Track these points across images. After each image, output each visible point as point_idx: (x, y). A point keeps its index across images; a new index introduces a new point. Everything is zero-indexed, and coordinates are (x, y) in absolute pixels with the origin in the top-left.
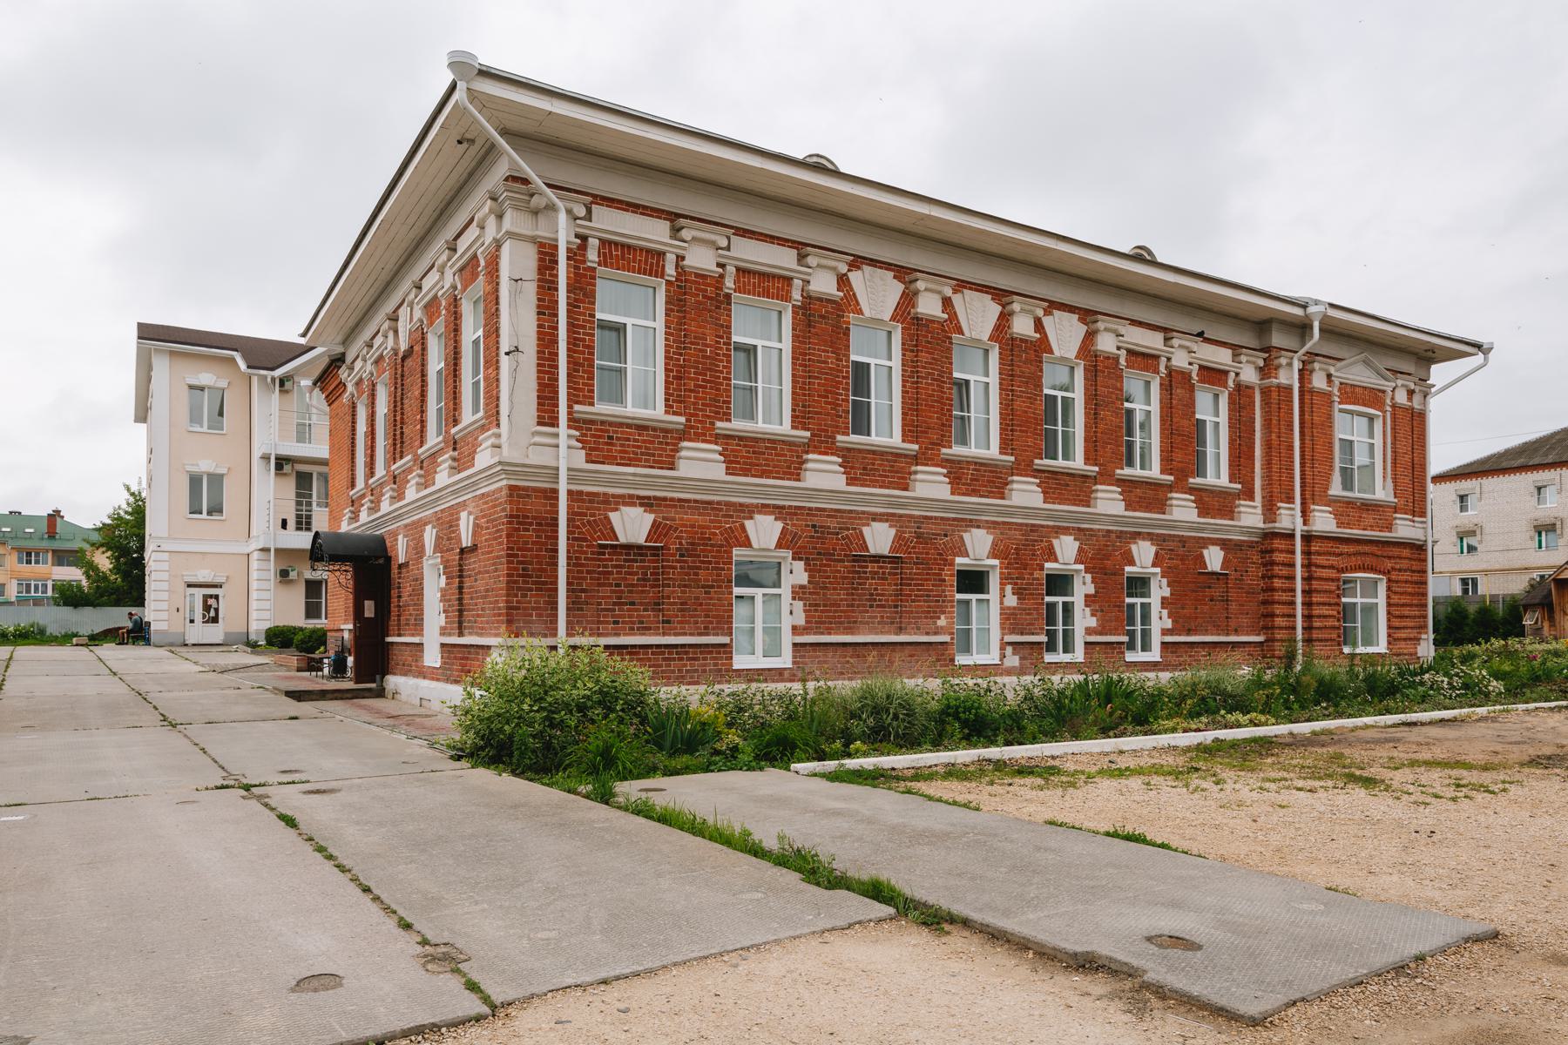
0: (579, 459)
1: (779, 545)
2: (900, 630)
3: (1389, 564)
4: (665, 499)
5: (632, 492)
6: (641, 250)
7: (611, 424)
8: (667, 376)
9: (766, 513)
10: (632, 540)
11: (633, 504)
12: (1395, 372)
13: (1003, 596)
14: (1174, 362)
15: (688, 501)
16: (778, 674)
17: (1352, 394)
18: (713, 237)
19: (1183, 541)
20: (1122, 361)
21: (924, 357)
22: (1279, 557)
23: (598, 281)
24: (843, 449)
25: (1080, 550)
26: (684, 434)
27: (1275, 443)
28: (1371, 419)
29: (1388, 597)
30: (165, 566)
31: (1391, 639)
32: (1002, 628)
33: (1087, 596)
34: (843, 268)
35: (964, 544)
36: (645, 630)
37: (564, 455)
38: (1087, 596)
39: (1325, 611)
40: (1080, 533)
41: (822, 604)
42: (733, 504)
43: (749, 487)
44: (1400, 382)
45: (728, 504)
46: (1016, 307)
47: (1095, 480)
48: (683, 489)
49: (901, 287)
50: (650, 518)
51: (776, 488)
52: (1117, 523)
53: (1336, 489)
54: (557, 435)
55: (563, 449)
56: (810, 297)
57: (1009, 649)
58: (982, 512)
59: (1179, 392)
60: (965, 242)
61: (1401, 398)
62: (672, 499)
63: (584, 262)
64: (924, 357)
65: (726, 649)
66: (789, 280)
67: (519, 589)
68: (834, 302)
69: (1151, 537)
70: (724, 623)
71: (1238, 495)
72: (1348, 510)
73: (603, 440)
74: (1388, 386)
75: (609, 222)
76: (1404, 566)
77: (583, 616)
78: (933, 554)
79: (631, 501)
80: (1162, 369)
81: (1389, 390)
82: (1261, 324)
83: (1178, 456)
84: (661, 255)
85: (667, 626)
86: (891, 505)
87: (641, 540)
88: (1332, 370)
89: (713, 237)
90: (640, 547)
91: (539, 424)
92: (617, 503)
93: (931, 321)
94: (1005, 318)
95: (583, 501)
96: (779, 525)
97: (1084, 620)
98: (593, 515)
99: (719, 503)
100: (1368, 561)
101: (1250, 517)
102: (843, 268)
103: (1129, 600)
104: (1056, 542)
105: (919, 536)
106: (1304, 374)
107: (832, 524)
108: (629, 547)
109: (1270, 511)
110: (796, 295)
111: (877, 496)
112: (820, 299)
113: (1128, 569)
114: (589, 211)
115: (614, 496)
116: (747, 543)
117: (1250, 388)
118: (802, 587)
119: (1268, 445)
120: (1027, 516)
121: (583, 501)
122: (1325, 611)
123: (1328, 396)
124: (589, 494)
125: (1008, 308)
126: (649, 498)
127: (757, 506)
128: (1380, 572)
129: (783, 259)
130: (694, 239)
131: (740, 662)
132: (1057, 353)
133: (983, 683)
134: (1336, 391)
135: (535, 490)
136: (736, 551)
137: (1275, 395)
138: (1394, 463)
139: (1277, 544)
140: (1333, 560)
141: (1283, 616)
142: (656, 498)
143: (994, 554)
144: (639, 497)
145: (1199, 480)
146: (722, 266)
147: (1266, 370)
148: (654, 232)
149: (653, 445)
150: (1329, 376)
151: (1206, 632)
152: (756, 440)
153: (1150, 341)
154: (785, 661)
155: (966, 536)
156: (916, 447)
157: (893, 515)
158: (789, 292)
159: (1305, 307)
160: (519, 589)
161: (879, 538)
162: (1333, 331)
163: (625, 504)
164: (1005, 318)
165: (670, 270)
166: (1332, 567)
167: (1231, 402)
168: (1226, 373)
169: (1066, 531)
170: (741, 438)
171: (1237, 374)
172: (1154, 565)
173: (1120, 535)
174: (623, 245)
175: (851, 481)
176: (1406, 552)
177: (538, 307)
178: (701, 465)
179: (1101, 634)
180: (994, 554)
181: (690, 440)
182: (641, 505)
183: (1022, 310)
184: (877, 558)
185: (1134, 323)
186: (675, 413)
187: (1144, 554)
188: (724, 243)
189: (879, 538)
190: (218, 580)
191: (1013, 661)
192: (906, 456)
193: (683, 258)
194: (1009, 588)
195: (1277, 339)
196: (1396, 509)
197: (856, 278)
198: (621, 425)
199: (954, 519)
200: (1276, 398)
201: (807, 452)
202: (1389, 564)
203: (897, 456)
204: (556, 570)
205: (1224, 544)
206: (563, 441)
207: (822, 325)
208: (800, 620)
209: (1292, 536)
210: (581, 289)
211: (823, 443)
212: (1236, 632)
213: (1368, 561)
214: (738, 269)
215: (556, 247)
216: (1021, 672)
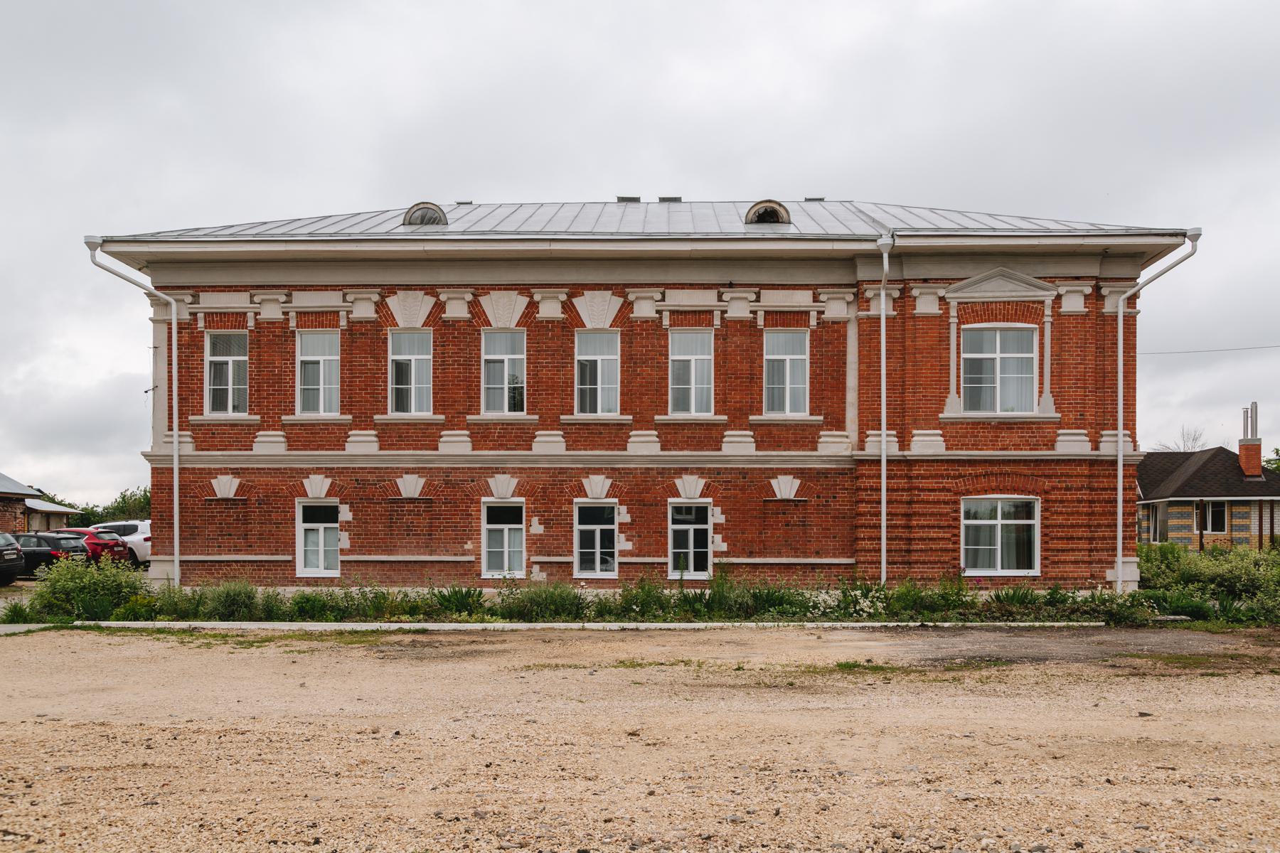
0: (189, 449)
3: (1048, 484)
12: (1051, 279)
16: (330, 581)
18: (744, 295)
19: (744, 473)
21: (451, 349)
31: (1043, 566)
35: (489, 487)
36: (238, 551)
40: (611, 472)
43: (304, 457)
45: (291, 469)
47: (631, 427)
48: (258, 462)
50: (236, 482)
53: (955, 408)
55: (1121, 444)
57: (536, 568)
58: (505, 462)
64: (451, 349)
65: (292, 564)
69: (701, 472)
70: (290, 547)
75: (212, 301)
79: (224, 472)
81: (1049, 302)
82: (850, 261)
85: (249, 549)
87: (231, 496)
89: (744, 295)
93: (456, 322)
96: (797, 482)
104: (585, 481)
106: (903, 301)
108: (227, 500)
110: (343, 323)
111: (407, 456)
114: (663, 294)
123: (941, 321)
131: (301, 572)
132: (589, 325)
133: (698, 591)
134: (953, 313)
139: (864, 470)
140: (946, 483)
150: (942, 299)
151: (779, 555)
152: (313, 425)
154: (336, 573)
158: (338, 321)
161: (411, 486)
165: (717, 322)
169: (597, 471)
170: (302, 425)
173: (662, 472)
175: (291, 447)
178: (455, 445)
179: (638, 556)
184: (411, 500)
195: (863, 273)
196: (1060, 424)
202: (1048, 484)
203: (620, 426)
207: (364, 343)
209: (1114, 463)
211: (643, 422)
213: (1008, 482)
214: (672, 312)
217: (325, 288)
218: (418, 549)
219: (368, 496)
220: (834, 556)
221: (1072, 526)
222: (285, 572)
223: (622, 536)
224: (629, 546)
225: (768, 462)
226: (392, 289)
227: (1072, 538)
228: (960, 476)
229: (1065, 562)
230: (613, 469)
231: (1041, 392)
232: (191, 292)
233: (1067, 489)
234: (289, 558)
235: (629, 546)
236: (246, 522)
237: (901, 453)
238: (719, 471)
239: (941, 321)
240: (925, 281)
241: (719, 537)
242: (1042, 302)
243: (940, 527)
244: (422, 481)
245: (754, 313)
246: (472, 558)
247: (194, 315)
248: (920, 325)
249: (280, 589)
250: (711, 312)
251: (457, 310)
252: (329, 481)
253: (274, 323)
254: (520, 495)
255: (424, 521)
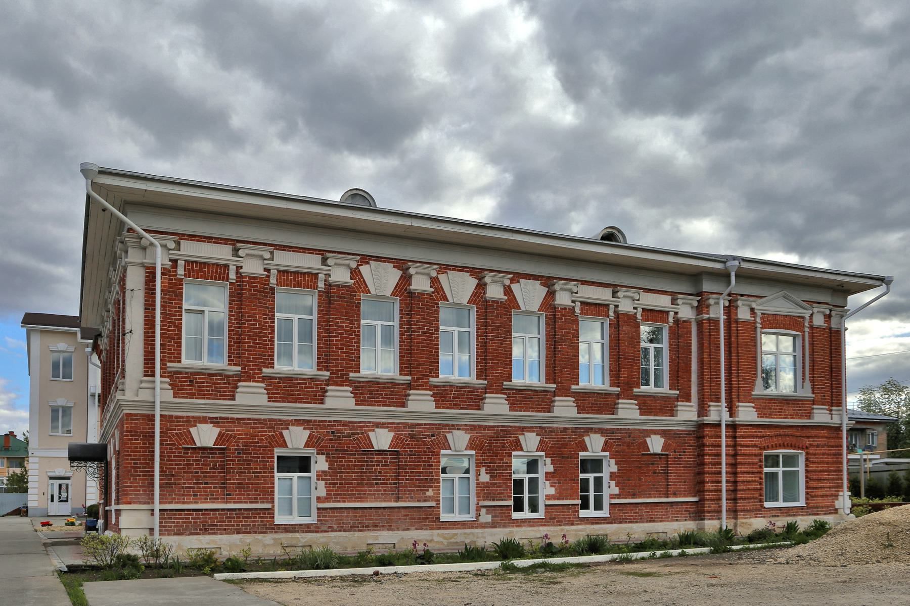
0: (169, 396)
1: (307, 445)
2: (397, 499)
4: (227, 418)
5: (205, 415)
6: (213, 264)
7: (192, 374)
8: (230, 342)
9: (297, 425)
10: (205, 445)
11: (206, 422)
13: (478, 475)
14: (621, 309)
15: (243, 419)
16: (307, 528)
17: (775, 322)
18: (260, 253)
19: (629, 432)
20: (578, 310)
22: (707, 441)
23: (440, 309)
24: (354, 382)
25: (541, 442)
26: (241, 378)
27: (706, 360)
28: (795, 337)
29: (807, 466)
30: (37, 466)
32: (478, 497)
33: (546, 473)
34: (507, 282)
36: (214, 500)
37: (161, 394)
38: (546, 473)
39: (749, 477)
40: (540, 431)
41: (337, 483)
42: (275, 420)
44: (815, 310)
45: (270, 420)
46: (557, 287)
48: (239, 412)
49: (477, 281)
50: (217, 431)
51: (467, 415)
52: (570, 422)
53: (759, 390)
54: (154, 382)
56: (330, 285)
57: (483, 511)
59: (624, 328)
60: (360, 228)
61: (819, 321)
62: (232, 419)
63: (176, 275)
65: (270, 512)
66: (316, 275)
67: (132, 475)
68: (348, 287)
69: (601, 431)
70: (269, 495)
71: (618, 396)
72: (768, 405)
73: (187, 384)
74: (806, 314)
76: (822, 443)
77: (174, 491)
78: (422, 448)
79: (204, 420)
80: (611, 313)
81: (807, 317)
82: (695, 276)
83: (624, 374)
84: (226, 267)
86: (390, 417)
88: (754, 305)
89: (347, 262)
90: (211, 449)
91: (145, 375)
92: (196, 422)
93: (421, 294)
94: (481, 286)
95: (173, 421)
97: (546, 489)
98: (180, 430)
99: (265, 420)
100: (788, 440)
101: (687, 413)
102: (507, 282)
103: (582, 476)
104: (521, 438)
105: (412, 436)
106: (730, 309)
107: (346, 431)
109: (703, 410)
112: (338, 286)
113: (581, 454)
114: (179, 244)
115: (193, 418)
116: (284, 445)
117: (687, 322)
118: (323, 472)
119: (701, 362)
120: (248, 412)
121: (173, 421)
122: (749, 477)
123: (752, 325)
124: (176, 417)
125: (552, 288)
126: (216, 418)
127: (291, 421)
128: (799, 448)
129: (311, 262)
130: (247, 255)
134: (758, 320)
135: (142, 415)
136: (276, 450)
137: (706, 325)
138: (812, 369)
139: (707, 431)
140: (756, 441)
141: (712, 482)
142: (221, 418)
143: (470, 447)
144: (210, 418)
145: (643, 388)
146: (635, 308)
147: (701, 307)
148: (220, 253)
149: (312, 390)
150: (752, 310)
151: (650, 496)
153: (602, 295)
154: (312, 520)
155: (449, 436)
156: (410, 378)
157: (393, 423)
159: (724, 262)
160: (132, 475)
161: (382, 439)
162: (744, 276)
163: (201, 422)
164: (481, 286)
166: (755, 446)
167: (672, 332)
168: (667, 312)
169: (530, 429)
170: (280, 378)
171: (676, 313)
172: (603, 450)
173: (575, 431)
174: (201, 263)
175: (512, 408)
176: (824, 433)
177: (145, 305)
178: (251, 397)
179: (558, 499)
180: (470, 447)
181: (244, 381)
182: (211, 422)
183: (493, 281)
184: (381, 452)
185: (584, 282)
186: (235, 365)
187: (595, 445)
188: (267, 256)
189: (382, 439)
190: (68, 475)
191: (486, 518)
192: (403, 384)
193: (241, 268)
194: (483, 470)
195: (707, 286)
196: (814, 402)
197: (364, 269)
198: (198, 374)
199: (440, 425)
200: (707, 328)
201: (328, 385)
204: (153, 464)
205: (664, 434)
206: (158, 385)
208: (323, 493)
210: (173, 292)
212: (675, 495)
213: (788, 440)
214: (279, 271)
215: (154, 268)
216: (493, 525)
217: (303, 250)
218: (385, 497)
219: (342, 446)
220: (685, 496)
221: (821, 471)
222: (263, 522)
223: (548, 483)
224: (552, 491)
225: (645, 424)
226: (365, 259)
227: (820, 480)
228: (763, 437)
229: (817, 496)
230: (540, 428)
231: (804, 379)
232: (511, 276)
233: (818, 446)
234: (269, 506)
235: (552, 491)
236: (223, 471)
237: (731, 419)
238: (612, 431)
239: (752, 325)
240: (819, 303)
241: (613, 483)
242: (803, 318)
243: (753, 473)
244: (392, 435)
245: (268, 270)
246: (433, 504)
247: (175, 262)
248: (740, 327)
249: (671, 551)
250: (608, 305)
251: (494, 292)
252: (307, 433)
253: (255, 278)
254: (543, 451)
255: (391, 472)
